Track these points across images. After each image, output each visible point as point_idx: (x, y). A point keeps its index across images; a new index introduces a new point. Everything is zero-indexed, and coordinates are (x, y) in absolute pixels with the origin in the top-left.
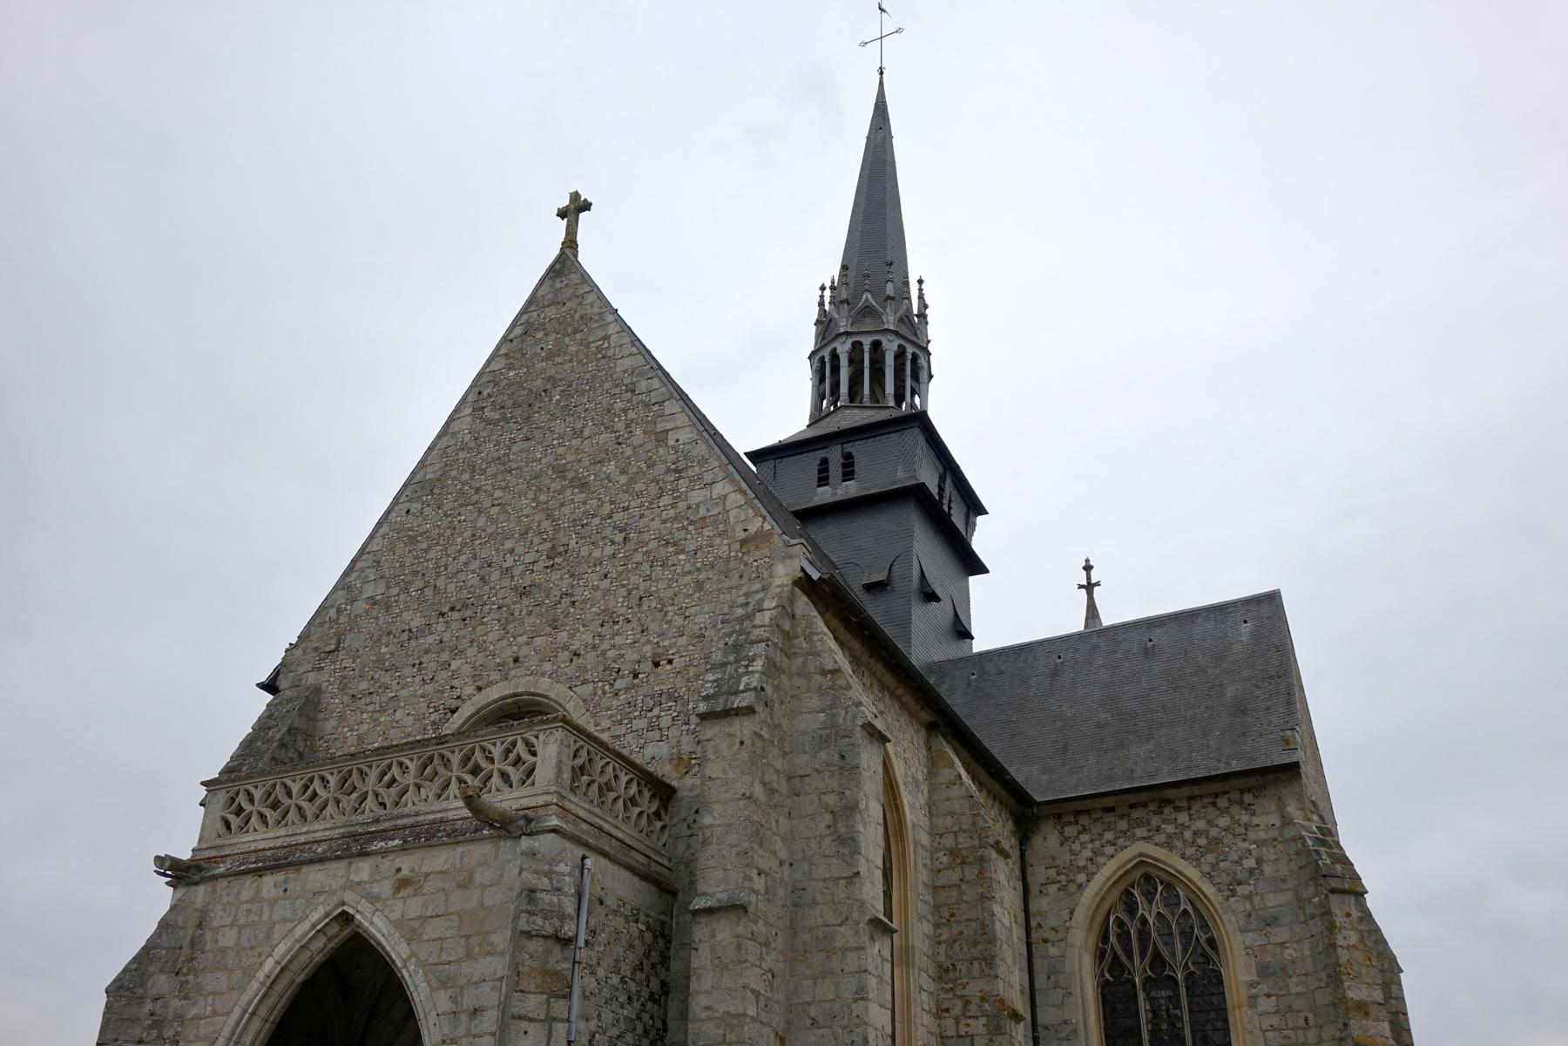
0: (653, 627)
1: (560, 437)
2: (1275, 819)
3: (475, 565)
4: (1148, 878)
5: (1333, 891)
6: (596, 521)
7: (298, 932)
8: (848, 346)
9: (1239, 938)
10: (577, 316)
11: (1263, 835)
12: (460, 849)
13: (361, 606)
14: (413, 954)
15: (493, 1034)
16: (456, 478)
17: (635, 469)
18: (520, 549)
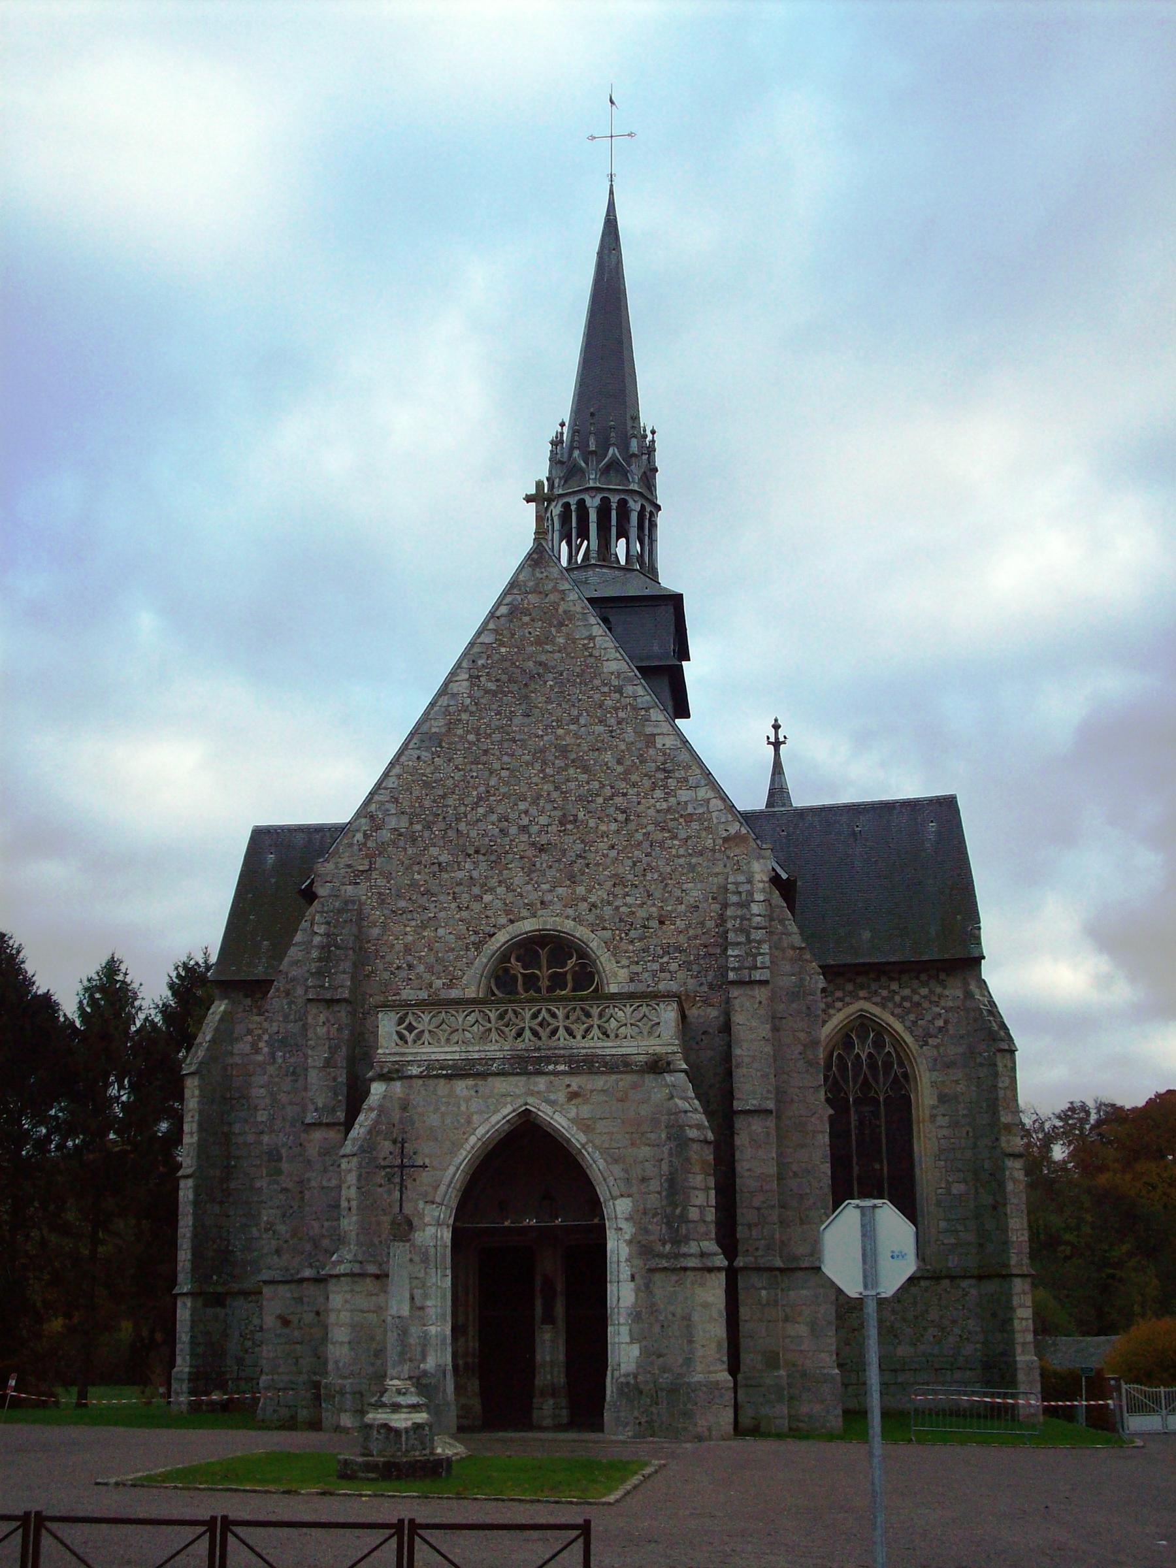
0: (657, 894)
1: (557, 721)
2: (959, 993)
3: (494, 817)
4: (863, 1025)
5: (1000, 1050)
6: (600, 800)
7: (494, 1119)
8: (597, 501)
9: (928, 1074)
10: (560, 611)
11: (950, 1004)
12: (614, 1077)
13: (385, 835)
14: (589, 1141)
15: (659, 1193)
16: (461, 737)
17: (629, 763)
18: (533, 811)
